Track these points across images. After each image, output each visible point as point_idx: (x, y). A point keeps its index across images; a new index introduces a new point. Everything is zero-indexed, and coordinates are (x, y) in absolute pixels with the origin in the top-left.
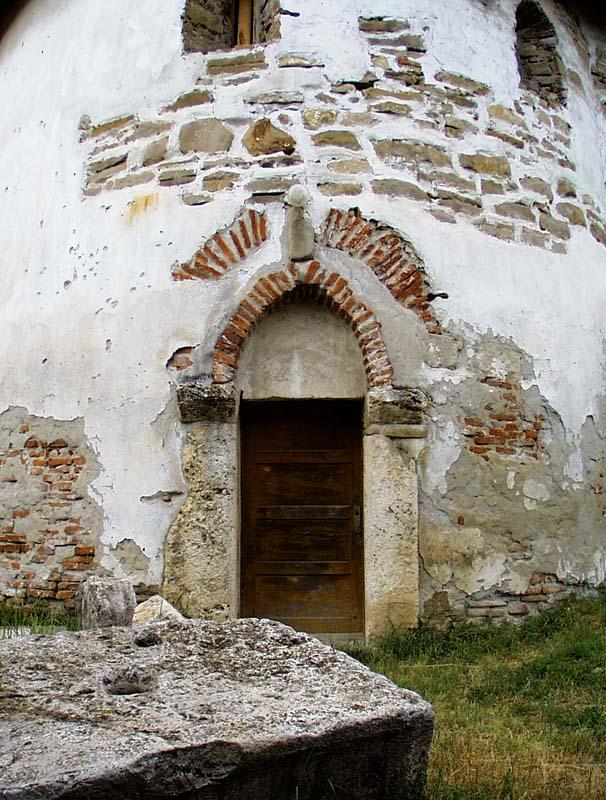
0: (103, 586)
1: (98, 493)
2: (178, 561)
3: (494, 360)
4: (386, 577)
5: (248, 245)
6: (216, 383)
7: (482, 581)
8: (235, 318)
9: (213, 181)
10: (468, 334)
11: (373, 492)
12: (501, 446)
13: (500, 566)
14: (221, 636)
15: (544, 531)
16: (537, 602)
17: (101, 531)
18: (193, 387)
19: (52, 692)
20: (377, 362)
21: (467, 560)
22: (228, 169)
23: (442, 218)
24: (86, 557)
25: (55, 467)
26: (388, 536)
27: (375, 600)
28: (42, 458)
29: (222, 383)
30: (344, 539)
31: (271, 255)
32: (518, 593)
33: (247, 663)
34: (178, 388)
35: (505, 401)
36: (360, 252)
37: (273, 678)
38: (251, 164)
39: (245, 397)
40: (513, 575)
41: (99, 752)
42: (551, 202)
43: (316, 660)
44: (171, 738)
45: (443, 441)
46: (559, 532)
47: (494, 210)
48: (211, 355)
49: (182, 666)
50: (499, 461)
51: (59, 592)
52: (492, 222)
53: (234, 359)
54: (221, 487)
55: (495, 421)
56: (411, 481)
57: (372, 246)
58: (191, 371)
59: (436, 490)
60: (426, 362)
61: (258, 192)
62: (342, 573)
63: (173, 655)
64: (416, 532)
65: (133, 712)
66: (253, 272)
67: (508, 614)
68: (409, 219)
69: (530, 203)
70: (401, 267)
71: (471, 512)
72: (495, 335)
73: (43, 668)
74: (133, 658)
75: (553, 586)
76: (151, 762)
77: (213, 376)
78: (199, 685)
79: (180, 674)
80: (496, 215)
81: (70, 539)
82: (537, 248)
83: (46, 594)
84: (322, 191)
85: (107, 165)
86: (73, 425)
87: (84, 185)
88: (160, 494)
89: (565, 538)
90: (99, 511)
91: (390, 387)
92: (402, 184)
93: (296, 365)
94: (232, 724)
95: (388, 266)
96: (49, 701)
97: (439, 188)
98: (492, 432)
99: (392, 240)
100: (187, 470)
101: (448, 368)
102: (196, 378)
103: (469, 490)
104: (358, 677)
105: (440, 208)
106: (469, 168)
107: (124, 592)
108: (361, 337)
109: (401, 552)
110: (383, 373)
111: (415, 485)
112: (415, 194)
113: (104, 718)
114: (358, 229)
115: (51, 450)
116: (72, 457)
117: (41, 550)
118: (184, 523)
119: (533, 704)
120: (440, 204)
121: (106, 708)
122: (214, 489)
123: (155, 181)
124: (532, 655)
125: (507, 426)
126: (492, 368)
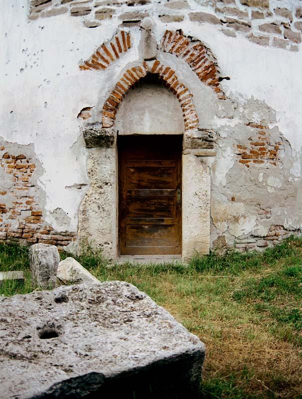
0: (42, 251)
1: (42, 184)
2: (85, 220)
3: (254, 113)
4: (195, 230)
5: (121, 51)
6: (104, 127)
7: (244, 230)
8: (114, 92)
9: (101, 14)
10: (241, 99)
11: (187, 185)
12: (256, 159)
13: (253, 222)
14: (99, 295)
15: (278, 203)
16: (273, 240)
17: (45, 203)
18: (92, 129)
19: (9, 338)
20: (190, 117)
21: (236, 219)
22: (109, 7)
23: (228, 34)
24: (37, 216)
25: (19, 169)
26: (194, 207)
27: (187, 240)
28: (12, 164)
29: (107, 128)
30: (172, 207)
31: (132, 58)
32: (262, 236)
33: (111, 314)
34: (84, 130)
35: (259, 135)
36: (182, 55)
37: (124, 325)
38: (122, 4)
39: (120, 134)
40: (260, 227)
41: (32, 382)
42: (291, 22)
43: (147, 313)
44: (69, 370)
45: (225, 157)
46: (286, 204)
47: (258, 28)
48: (101, 112)
49: (78, 317)
50: (254, 167)
51: (24, 234)
52: (256, 35)
53: (113, 115)
54: (107, 182)
55: (254, 146)
56: (207, 178)
57: (188, 51)
58: (91, 121)
59: (221, 184)
60: (216, 115)
61: (125, 20)
62: (171, 224)
63: (74, 310)
64: (209, 205)
65: (51, 352)
66: (123, 66)
67: (257, 248)
68: (211, 36)
69: (279, 23)
70: (204, 63)
71: (238, 194)
72: (255, 99)
73: (5, 321)
74: (52, 312)
75: (281, 232)
76: (58, 386)
77: (102, 123)
78: (86, 331)
79: (76, 323)
80: (259, 31)
81: (29, 207)
82: (282, 49)
83: (17, 235)
84: (162, 20)
85: (41, 3)
86: (27, 147)
87: (28, 14)
88: (75, 185)
89: (289, 207)
90: (44, 193)
91: (197, 130)
92: (206, 15)
93: (147, 117)
94: (101, 360)
95: (197, 63)
96: (7, 345)
97: (228, 16)
98: (251, 152)
99: (200, 47)
100: (89, 173)
101: (229, 118)
102: (93, 124)
103: (237, 183)
104: (167, 326)
105: (228, 28)
106: (245, 4)
107: (53, 253)
108: (182, 102)
109: (202, 216)
110: (193, 122)
111: (209, 181)
112: (214, 21)
113: (35, 356)
114: (181, 42)
115: (17, 160)
116: (29, 164)
117: (14, 212)
118: (88, 200)
119: (265, 304)
120: (228, 26)
121: (37, 349)
122: (103, 183)
123: (69, 13)
124: (267, 271)
125: (259, 150)
126: (253, 118)
